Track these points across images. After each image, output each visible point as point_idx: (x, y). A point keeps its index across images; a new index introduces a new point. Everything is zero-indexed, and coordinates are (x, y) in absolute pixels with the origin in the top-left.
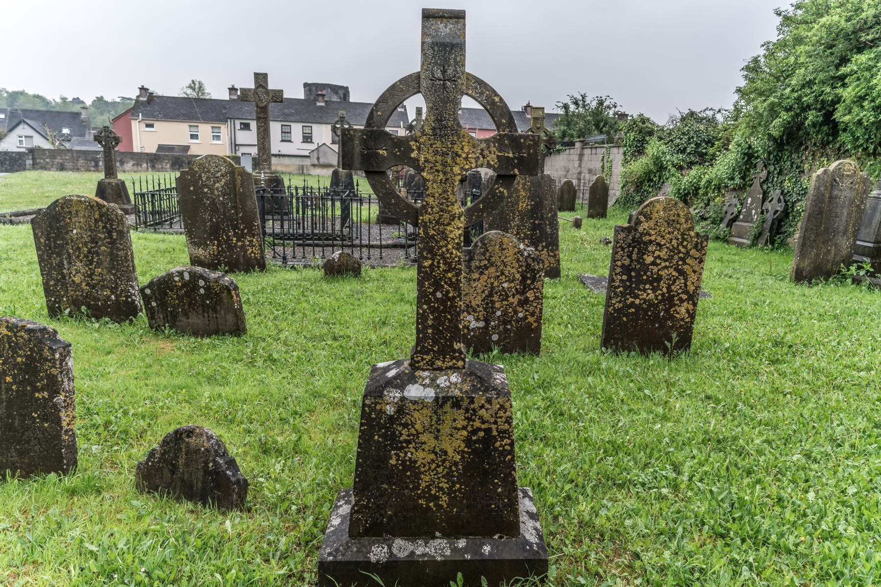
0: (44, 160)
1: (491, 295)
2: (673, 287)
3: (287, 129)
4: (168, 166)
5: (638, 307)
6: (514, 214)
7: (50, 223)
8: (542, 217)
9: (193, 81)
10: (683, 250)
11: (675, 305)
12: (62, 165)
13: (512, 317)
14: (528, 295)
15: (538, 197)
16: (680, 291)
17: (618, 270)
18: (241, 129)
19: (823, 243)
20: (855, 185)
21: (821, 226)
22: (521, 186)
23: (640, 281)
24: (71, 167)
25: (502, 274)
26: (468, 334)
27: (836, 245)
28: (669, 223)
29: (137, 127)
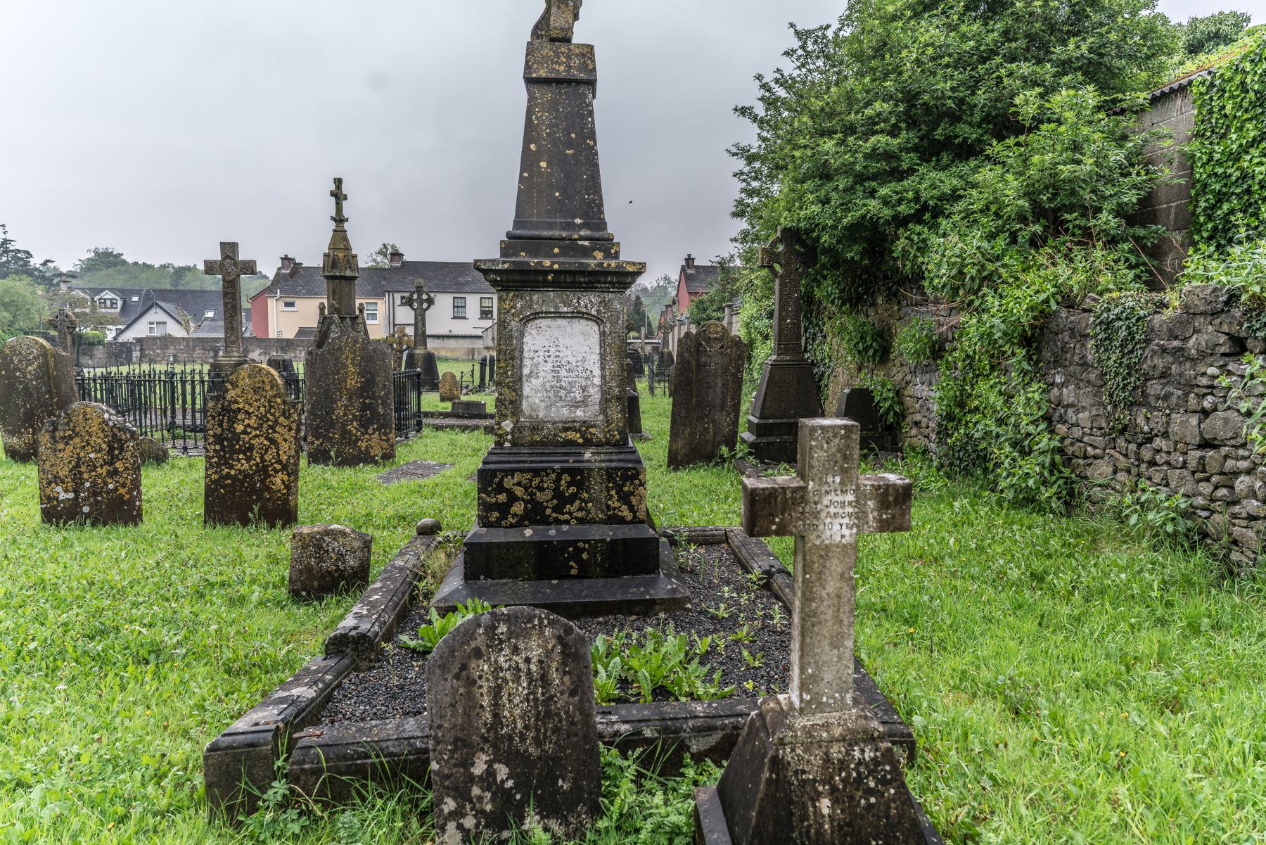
0: (154, 351)
1: (77, 465)
2: (266, 457)
3: (459, 303)
5: (234, 478)
6: (341, 393)
9: (384, 245)
10: (271, 418)
13: (102, 488)
14: (117, 465)
15: (370, 373)
16: (273, 461)
17: (211, 440)
18: (402, 304)
19: (698, 420)
22: (350, 361)
23: (233, 451)
25: (88, 444)
26: (58, 505)
27: (714, 422)
29: (274, 306)
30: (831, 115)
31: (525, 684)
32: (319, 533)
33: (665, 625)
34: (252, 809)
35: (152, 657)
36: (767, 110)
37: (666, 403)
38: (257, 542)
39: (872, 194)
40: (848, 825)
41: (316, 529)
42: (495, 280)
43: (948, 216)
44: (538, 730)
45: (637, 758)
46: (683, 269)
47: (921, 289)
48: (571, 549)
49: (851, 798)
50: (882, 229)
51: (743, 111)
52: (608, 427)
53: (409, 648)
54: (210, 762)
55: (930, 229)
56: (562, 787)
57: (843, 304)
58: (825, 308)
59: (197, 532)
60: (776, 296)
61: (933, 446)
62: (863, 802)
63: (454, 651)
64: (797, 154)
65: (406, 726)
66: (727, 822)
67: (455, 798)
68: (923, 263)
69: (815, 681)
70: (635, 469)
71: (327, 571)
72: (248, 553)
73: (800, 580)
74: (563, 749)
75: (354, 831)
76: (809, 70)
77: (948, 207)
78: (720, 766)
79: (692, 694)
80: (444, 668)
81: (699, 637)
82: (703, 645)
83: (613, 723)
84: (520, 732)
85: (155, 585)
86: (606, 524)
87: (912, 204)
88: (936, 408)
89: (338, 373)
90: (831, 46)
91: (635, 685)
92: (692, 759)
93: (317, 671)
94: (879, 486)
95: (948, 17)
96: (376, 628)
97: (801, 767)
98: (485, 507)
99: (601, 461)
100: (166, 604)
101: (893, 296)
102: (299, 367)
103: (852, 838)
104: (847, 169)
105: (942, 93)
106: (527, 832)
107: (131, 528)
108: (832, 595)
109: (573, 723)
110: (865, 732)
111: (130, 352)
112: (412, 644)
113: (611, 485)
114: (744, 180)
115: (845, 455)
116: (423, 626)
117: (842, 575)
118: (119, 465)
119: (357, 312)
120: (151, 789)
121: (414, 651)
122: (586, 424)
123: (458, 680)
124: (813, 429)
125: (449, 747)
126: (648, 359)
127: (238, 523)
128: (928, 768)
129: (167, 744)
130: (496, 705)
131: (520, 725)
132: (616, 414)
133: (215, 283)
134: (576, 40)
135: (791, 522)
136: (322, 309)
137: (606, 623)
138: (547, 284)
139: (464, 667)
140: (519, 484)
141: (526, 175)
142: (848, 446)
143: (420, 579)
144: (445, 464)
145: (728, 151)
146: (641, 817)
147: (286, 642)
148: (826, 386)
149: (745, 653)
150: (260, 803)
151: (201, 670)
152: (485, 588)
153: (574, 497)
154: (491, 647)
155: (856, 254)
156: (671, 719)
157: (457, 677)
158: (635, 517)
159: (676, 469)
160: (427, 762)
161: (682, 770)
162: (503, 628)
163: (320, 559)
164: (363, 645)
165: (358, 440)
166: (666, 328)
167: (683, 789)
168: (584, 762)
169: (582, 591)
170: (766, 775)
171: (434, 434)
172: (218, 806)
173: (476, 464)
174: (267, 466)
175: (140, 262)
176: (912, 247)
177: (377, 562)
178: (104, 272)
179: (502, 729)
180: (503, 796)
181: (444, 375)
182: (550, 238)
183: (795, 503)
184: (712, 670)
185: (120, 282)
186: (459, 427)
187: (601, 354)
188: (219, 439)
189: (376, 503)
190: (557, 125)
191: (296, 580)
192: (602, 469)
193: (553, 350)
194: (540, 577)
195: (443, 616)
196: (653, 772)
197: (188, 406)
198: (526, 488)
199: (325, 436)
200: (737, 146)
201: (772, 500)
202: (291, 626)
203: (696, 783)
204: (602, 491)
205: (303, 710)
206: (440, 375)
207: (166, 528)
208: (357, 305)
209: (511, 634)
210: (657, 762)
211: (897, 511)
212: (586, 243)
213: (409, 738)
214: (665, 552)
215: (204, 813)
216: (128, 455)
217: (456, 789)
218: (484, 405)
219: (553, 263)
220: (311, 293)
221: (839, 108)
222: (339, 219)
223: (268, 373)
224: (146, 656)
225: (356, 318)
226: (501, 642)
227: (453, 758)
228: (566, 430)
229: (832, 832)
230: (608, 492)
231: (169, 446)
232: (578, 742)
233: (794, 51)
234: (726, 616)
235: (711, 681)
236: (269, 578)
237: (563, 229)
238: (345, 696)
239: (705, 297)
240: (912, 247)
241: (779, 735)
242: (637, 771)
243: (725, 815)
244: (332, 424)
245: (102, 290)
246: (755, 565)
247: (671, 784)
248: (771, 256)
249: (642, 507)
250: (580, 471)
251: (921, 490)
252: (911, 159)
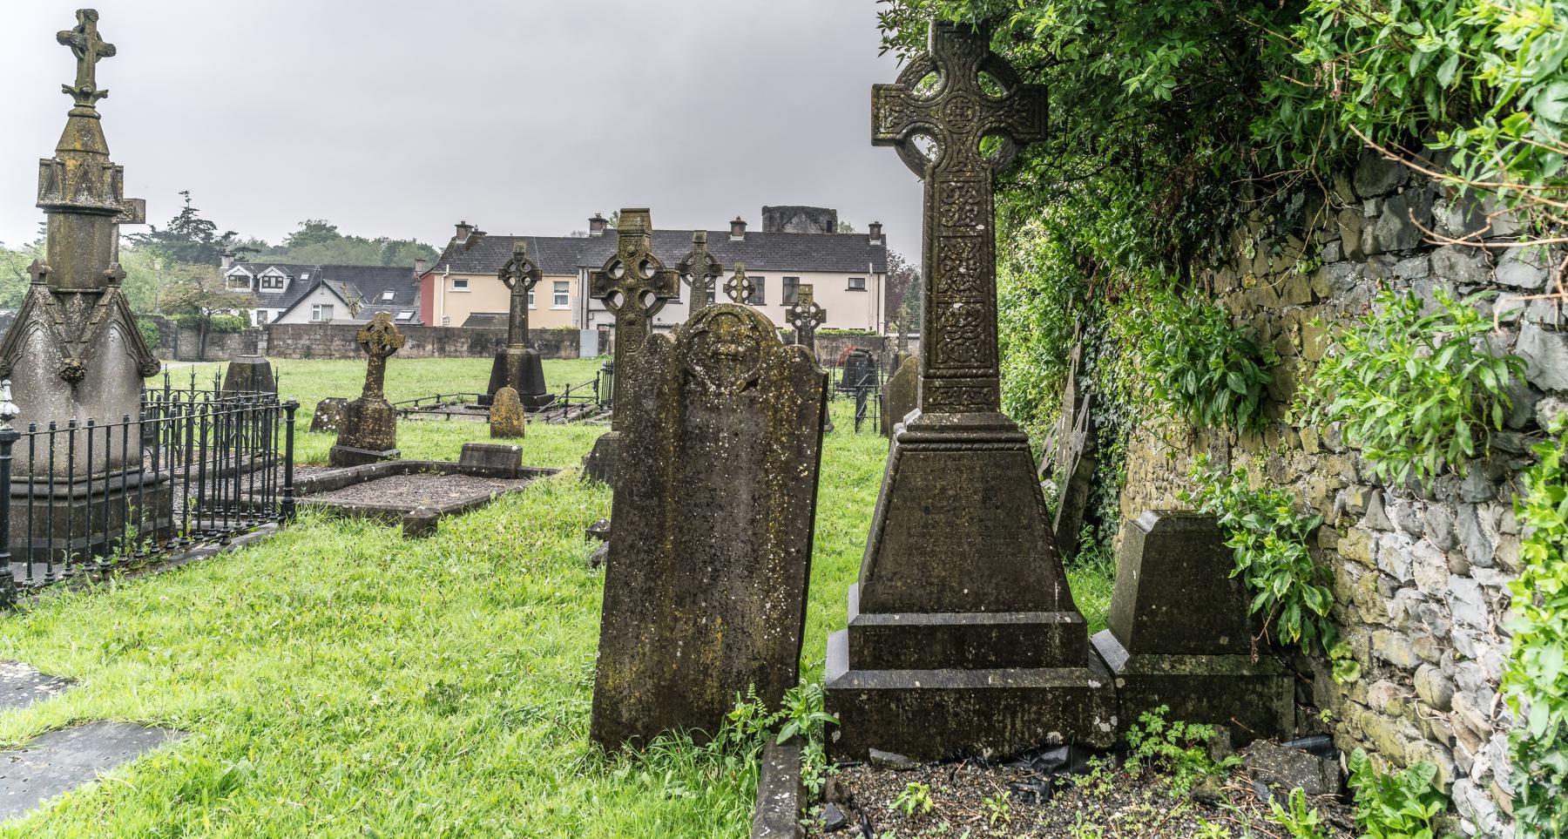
4: (465, 348)
7: (1449, 422)
12: (309, 348)
19: (680, 601)
20: (765, 390)
21: (661, 538)
24: (322, 352)
27: (726, 611)
148: (1122, 457)
175: (354, 236)
222: (85, 92)
245: (267, 266)
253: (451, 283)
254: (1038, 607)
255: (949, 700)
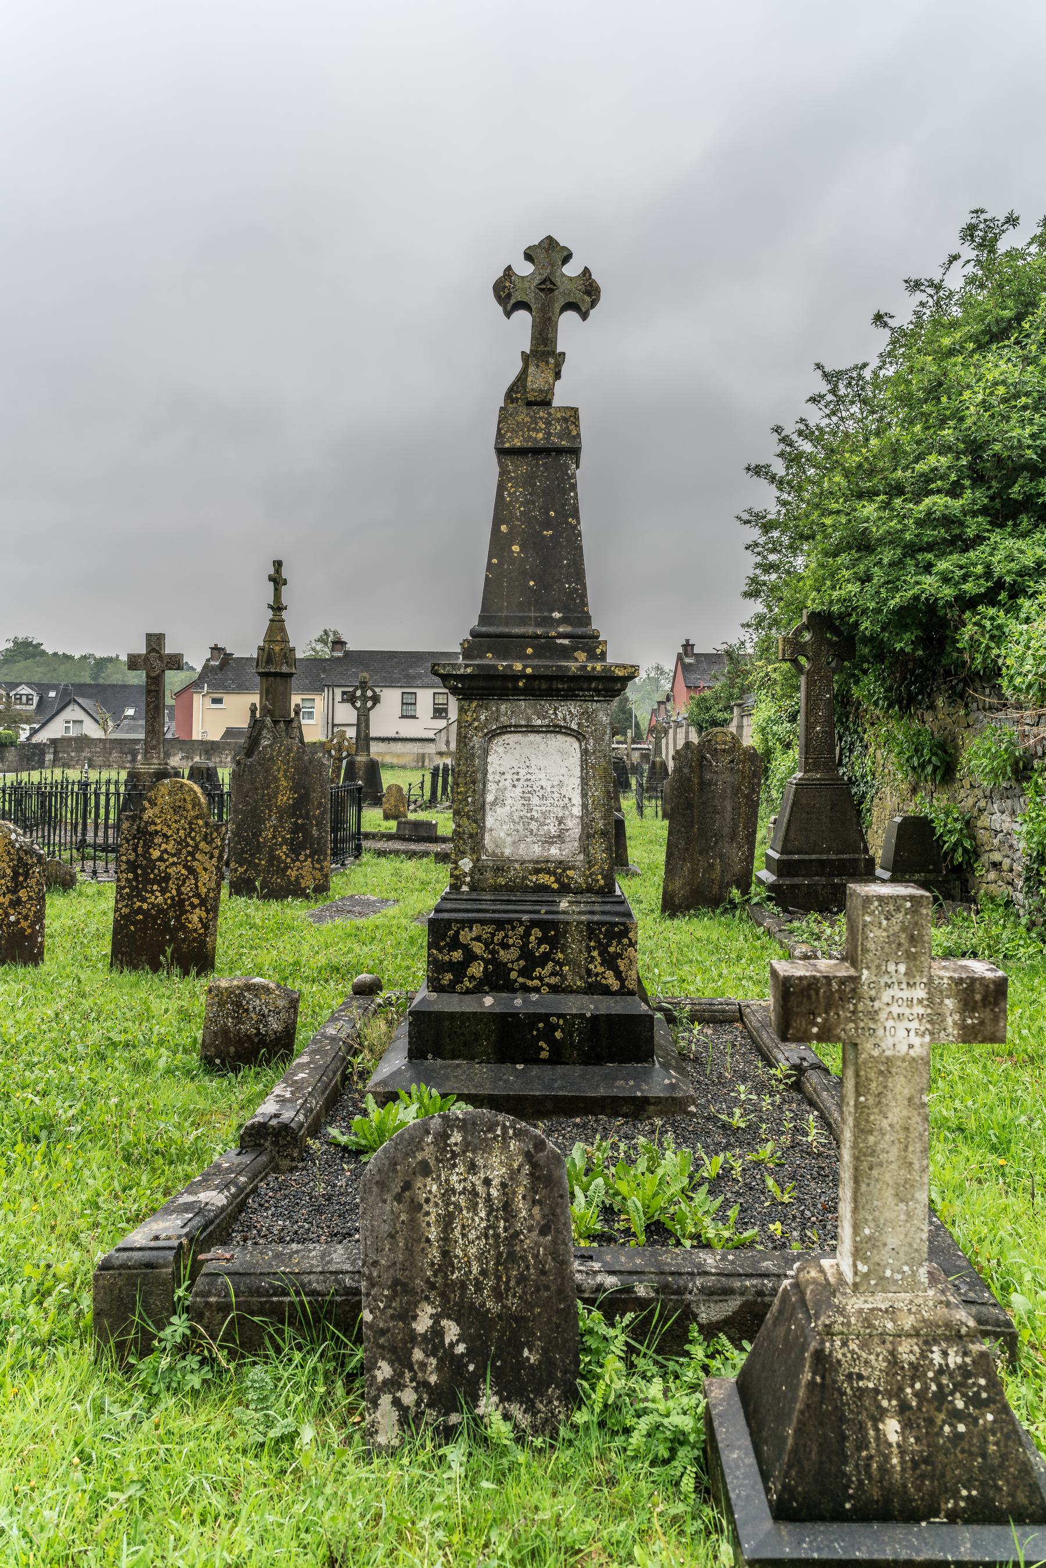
8: (307, 814)
9: (326, 632)
11: (187, 911)
18: (343, 701)
19: (701, 854)
21: (692, 827)
23: (147, 881)
27: (721, 856)
28: (176, 810)
29: (200, 703)
30: (871, 473)
31: (483, 1214)
32: (238, 987)
33: (661, 1133)
34: (146, 1350)
35: (43, 1135)
36: (787, 468)
37: (660, 828)
38: (168, 993)
39: (928, 568)
40: (926, 1461)
41: (235, 983)
42: (456, 687)
43: (1033, 596)
44: (499, 1278)
45: (627, 1326)
46: (680, 658)
47: (997, 689)
48: (541, 1025)
49: (930, 1421)
50: (941, 613)
51: (758, 470)
52: (589, 869)
53: (338, 1145)
54: (101, 1283)
55: (1007, 612)
56: (528, 1359)
57: (890, 706)
58: (866, 711)
59: (102, 977)
60: (801, 695)
61: (1020, 896)
62: (947, 1429)
63: (395, 1164)
64: (828, 521)
65: (334, 1256)
66: (751, 1435)
67: (391, 1363)
68: (998, 656)
69: (874, 1246)
70: (623, 924)
71: (246, 1035)
72: (157, 1006)
73: (852, 1103)
74: (530, 1306)
75: (265, 1393)
76: (842, 419)
77: (1032, 584)
78: (742, 1349)
79: (700, 1236)
80: (382, 1185)
81: (706, 1154)
82: (712, 1167)
83: (595, 1273)
84: (476, 1279)
85: (52, 1041)
86: (586, 993)
87: (982, 581)
88: (1022, 845)
89: (268, 787)
90: (869, 389)
91: (623, 1217)
92: (700, 1332)
93: (229, 1170)
94: (961, 979)
95: (1023, 348)
96: (301, 1117)
97: (856, 1370)
98: (436, 967)
99: (580, 913)
100: (63, 1067)
101: (958, 697)
102: (224, 775)
103: (932, 1482)
104: (893, 539)
105: (1019, 441)
106: (482, 1418)
107: (30, 968)
108: (897, 1127)
109: (543, 1272)
110: (948, 1325)
111: (43, 754)
112: (343, 1139)
113: (592, 944)
114: (759, 554)
115: (912, 936)
116: (358, 1117)
117: (910, 1100)
118: (23, 894)
119: (293, 715)
120: (32, 1311)
121: (345, 1149)
122: (563, 865)
123: (399, 1202)
124: (867, 900)
125: (386, 1292)
126: (636, 770)
127: (147, 967)
128: (1037, 1375)
129: (53, 1250)
130: (446, 1239)
131: (475, 1269)
132: (600, 853)
133: (138, 678)
134: (556, 402)
135: (838, 1024)
136: (253, 711)
137: (584, 1126)
138: (517, 692)
139: (407, 1186)
140: (478, 939)
141: (495, 561)
142: (916, 923)
143: (355, 1054)
144: (387, 900)
145: (739, 518)
146: (632, 1412)
147: (196, 1125)
148: (869, 810)
149: (770, 1182)
150: (156, 1343)
151: (97, 1155)
152: (433, 1071)
153: (545, 958)
154: (441, 1161)
155: (906, 644)
156: (672, 1274)
157: (399, 1198)
158: (623, 986)
159: (672, 916)
160: (357, 1307)
161: (687, 1347)
162: (456, 1137)
163: (239, 1020)
164: (284, 1138)
165: (287, 868)
166: (659, 732)
167: (689, 1375)
168: (558, 1326)
169: (555, 1080)
170: (807, 1376)
171: (375, 861)
172: (107, 1342)
173: (428, 902)
174: (184, 900)
176: (983, 635)
177: (304, 1025)
178: (21, 665)
179: (453, 1273)
180: (450, 1363)
181: (389, 788)
182: (523, 636)
183: (844, 998)
184: (726, 1205)
185: (38, 674)
186: (406, 852)
187: (582, 778)
188: (132, 866)
189: (306, 948)
190: (533, 502)
191: (210, 1045)
192: (582, 922)
193: (522, 772)
194: (501, 1061)
195: (382, 1105)
196: (648, 1348)
197: (101, 820)
198: (487, 945)
199: (250, 863)
200: (750, 511)
201: (812, 993)
202: (202, 1104)
203: (706, 1369)
204: (581, 952)
205: (212, 1222)
206: (385, 786)
207: (68, 970)
208: (293, 707)
209: (466, 1146)
210: (653, 1333)
211: (987, 1015)
212: (566, 642)
213: (336, 1273)
214: (661, 1032)
215: (89, 1349)
216: (32, 882)
217: (393, 1350)
218: (436, 825)
219: (525, 667)
220: (242, 688)
221: (881, 464)
222: (277, 607)
223: (191, 789)
224: (37, 1132)
225: (292, 721)
226: (454, 1155)
227: (390, 1307)
228: (537, 871)
229: (903, 1470)
230: (589, 952)
231: (78, 869)
232: (550, 1298)
233: (822, 397)
234: (743, 1125)
235: (725, 1219)
236: (178, 1040)
237: (538, 625)
238: (261, 1205)
239: (707, 693)
240: (983, 635)
241: (824, 1320)
242: (627, 1344)
243: (749, 1425)
244: (259, 848)
245: (18, 685)
246: (780, 1056)
247: (671, 1365)
248: (795, 647)
249: (633, 974)
250: (553, 924)
251: (1005, 956)
252: (979, 524)
253: (208, 700)
254: (854, 852)
255: (819, 888)
